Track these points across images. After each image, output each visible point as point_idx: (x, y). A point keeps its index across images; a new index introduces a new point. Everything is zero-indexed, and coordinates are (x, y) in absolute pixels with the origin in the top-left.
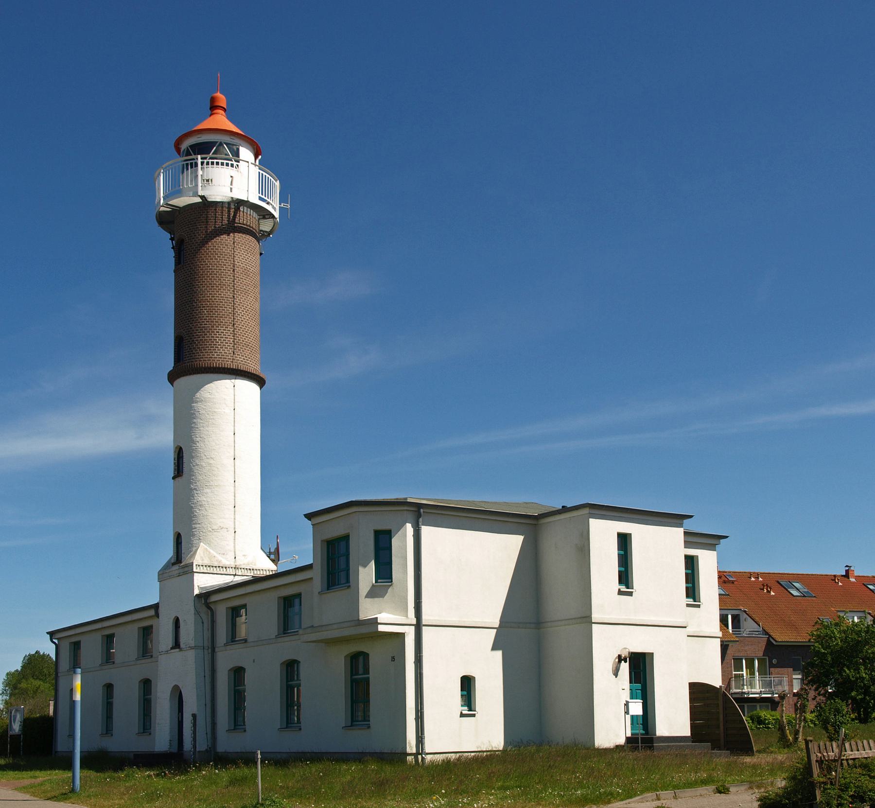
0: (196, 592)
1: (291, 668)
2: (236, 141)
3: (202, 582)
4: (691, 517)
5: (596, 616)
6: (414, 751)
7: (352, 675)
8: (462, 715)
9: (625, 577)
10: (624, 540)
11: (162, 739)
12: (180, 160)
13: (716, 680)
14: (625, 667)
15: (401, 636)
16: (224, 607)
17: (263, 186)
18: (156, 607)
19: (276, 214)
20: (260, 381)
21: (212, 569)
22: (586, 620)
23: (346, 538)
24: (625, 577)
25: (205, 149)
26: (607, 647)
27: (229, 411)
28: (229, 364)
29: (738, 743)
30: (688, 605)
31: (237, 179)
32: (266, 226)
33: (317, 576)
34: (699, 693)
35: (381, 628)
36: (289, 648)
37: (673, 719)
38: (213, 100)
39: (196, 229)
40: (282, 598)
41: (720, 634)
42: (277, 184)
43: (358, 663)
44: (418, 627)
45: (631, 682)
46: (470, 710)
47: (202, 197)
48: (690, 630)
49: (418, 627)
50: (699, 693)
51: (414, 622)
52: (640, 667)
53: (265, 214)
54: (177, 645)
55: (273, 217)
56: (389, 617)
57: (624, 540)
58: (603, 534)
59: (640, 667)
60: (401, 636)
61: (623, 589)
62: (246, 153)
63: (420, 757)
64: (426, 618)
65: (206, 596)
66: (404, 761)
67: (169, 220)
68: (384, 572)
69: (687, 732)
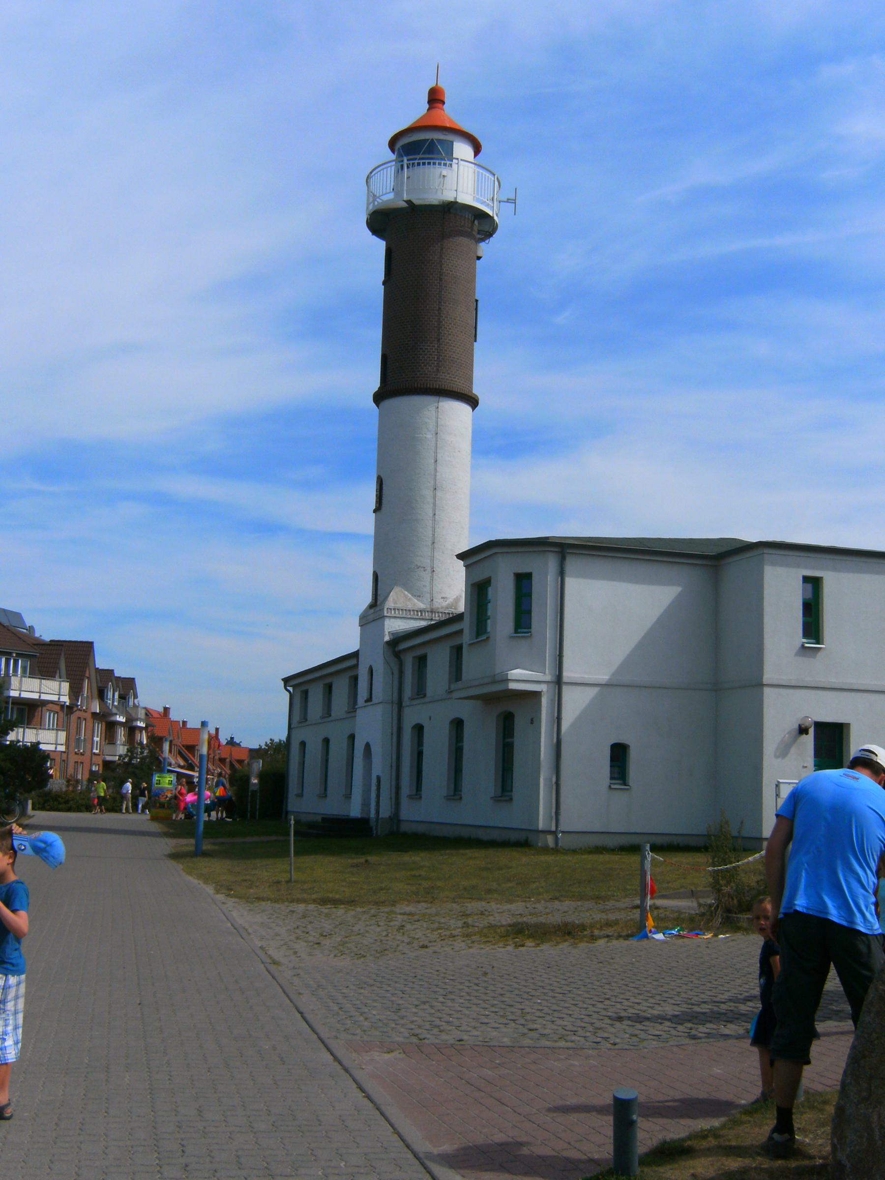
1: (458, 724)
2: (449, 137)
3: (394, 626)
7: (504, 737)
14: (809, 740)
18: (355, 655)
35: (513, 686)
43: (507, 723)
54: (369, 699)
56: (521, 676)
60: (537, 695)
62: (462, 150)
64: (567, 675)
65: (397, 640)
68: (523, 620)
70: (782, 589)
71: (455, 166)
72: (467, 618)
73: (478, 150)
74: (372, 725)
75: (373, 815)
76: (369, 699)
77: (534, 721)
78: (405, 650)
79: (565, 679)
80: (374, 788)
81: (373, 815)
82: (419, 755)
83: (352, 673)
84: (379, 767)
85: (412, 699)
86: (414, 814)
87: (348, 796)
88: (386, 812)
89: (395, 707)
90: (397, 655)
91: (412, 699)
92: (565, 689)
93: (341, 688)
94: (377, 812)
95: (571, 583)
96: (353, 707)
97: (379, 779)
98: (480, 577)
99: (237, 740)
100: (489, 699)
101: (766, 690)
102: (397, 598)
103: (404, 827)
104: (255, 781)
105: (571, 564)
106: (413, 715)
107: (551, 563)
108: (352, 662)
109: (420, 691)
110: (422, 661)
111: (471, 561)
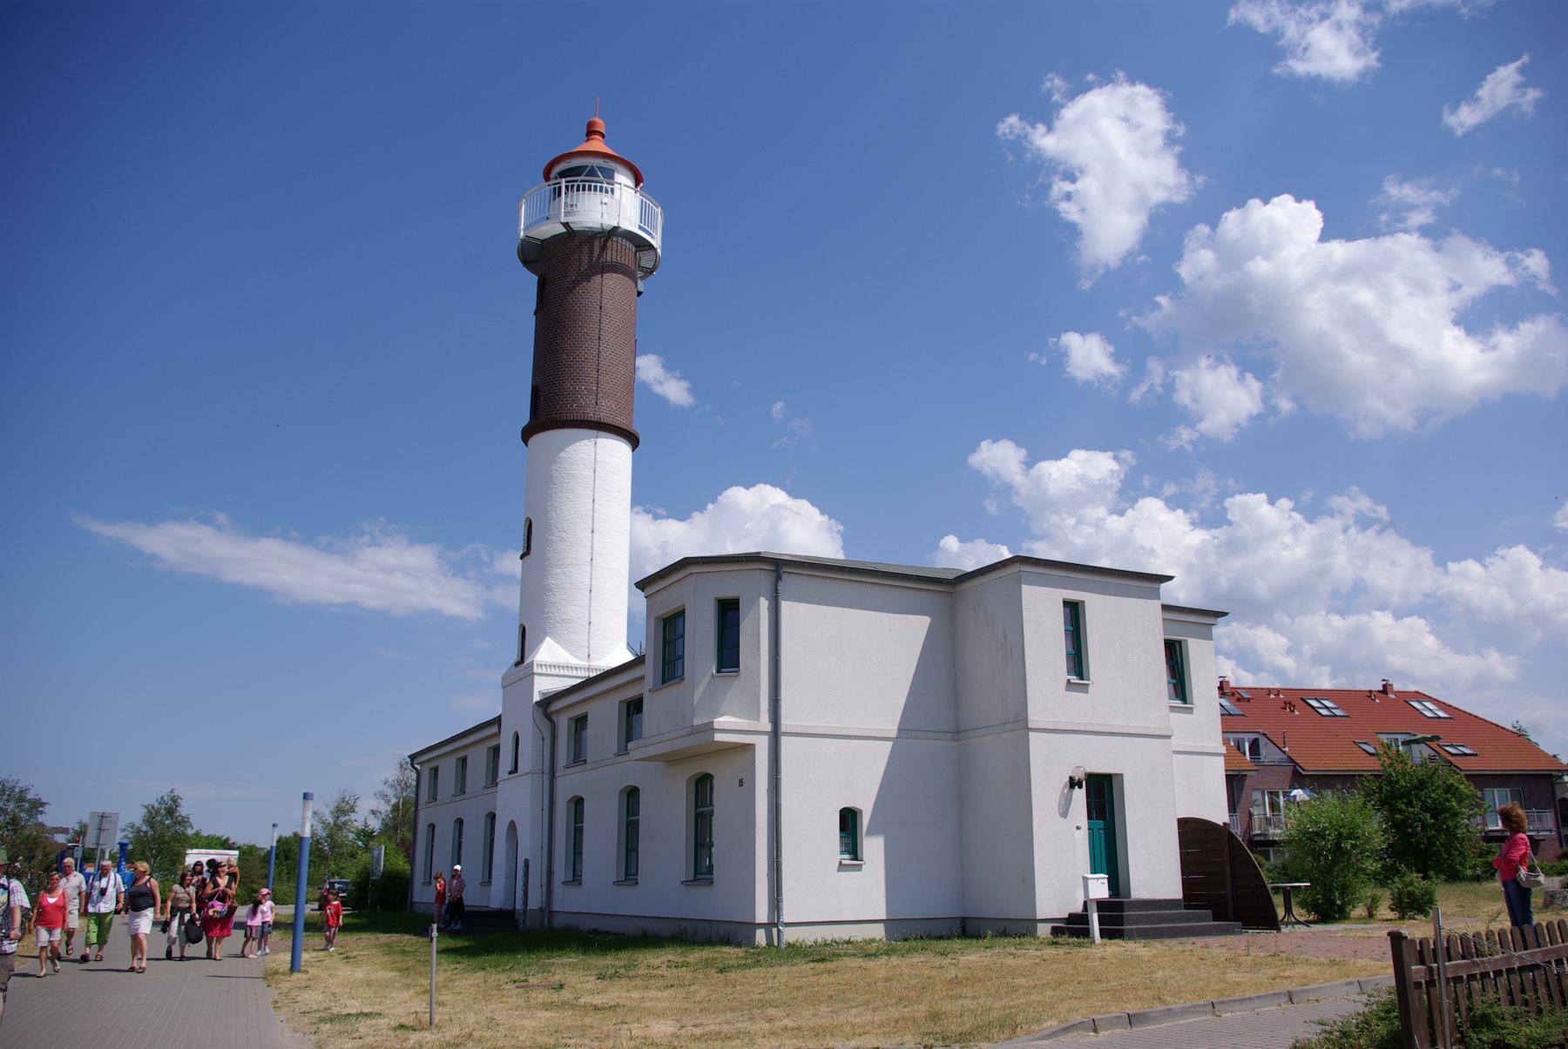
0: (537, 698)
1: (632, 795)
2: (612, 165)
3: (544, 686)
4: (1225, 614)
5: (1035, 716)
6: (765, 921)
7: (697, 807)
8: (842, 867)
9: (1077, 662)
10: (1074, 611)
11: (496, 898)
12: (545, 188)
13: (1216, 810)
14: (1080, 795)
15: (749, 748)
16: (565, 714)
17: (644, 213)
18: (497, 721)
19: (656, 242)
20: (633, 440)
21: (554, 669)
22: (1020, 724)
23: (681, 614)
24: (1077, 662)
25: (573, 173)
26: (1051, 766)
27: (588, 473)
28: (592, 416)
29: (1251, 911)
30: (1172, 708)
31: (618, 206)
32: (647, 261)
33: (649, 670)
34: (1193, 833)
35: (719, 737)
36: (630, 771)
37: (1156, 872)
38: (590, 124)
39: (565, 268)
40: (622, 698)
41: (1223, 750)
42: (659, 210)
43: (702, 786)
44: (775, 735)
45: (1090, 818)
46: (856, 858)
47: (566, 225)
48: (1176, 743)
49: (775, 735)
50: (1193, 833)
51: (768, 727)
52: (1102, 795)
53: (643, 245)
54: (515, 770)
55: (652, 247)
56: (729, 724)
57: (1074, 611)
58: (1041, 608)
59: (1102, 795)
60: (749, 748)
61: (1074, 679)
62: (623, 179)
63: (775, 930)
64: (786, 723)
65: (547, 701)
66: (749, 941)
67: (535, 254)
68: (728, 657)
69: (1174, 891)
70: (1041, 608)
71: (617, 191)
72: (649, 661)
73: (638, 180)
74: (517, 800)
75: (519, 906)
76: (515, 770)
77: (745, 783)
78: (558, 711)
79: (783, 729)
80: (520, 874)
81: (519, 906)
82: (578, 832)
83: (493, 743)
84: (528, 846)
85: (566, 767)
86: (568, 901)
87: (488, 881)
88: (535, 902)
89: (547, 777)
90: (548, 717)
91: (566, 767)
92: (784, 740)
93: (478, 759)
94: (526, 904)
95: (786, 607)
96: (493, 780)
97: (527, 863)
98: (668, 608)
99: (183, 811)
100: (673, 759)
101: (1031, 734)
102: (548, 653)
103: (558, 922)
104: (1453, 190)
105: (789, 582)
106: (570, 783)
107: (763, 579)
108: (494, 729)
109: (578, 758)
110: (580, 722)
111: (650, 590)
